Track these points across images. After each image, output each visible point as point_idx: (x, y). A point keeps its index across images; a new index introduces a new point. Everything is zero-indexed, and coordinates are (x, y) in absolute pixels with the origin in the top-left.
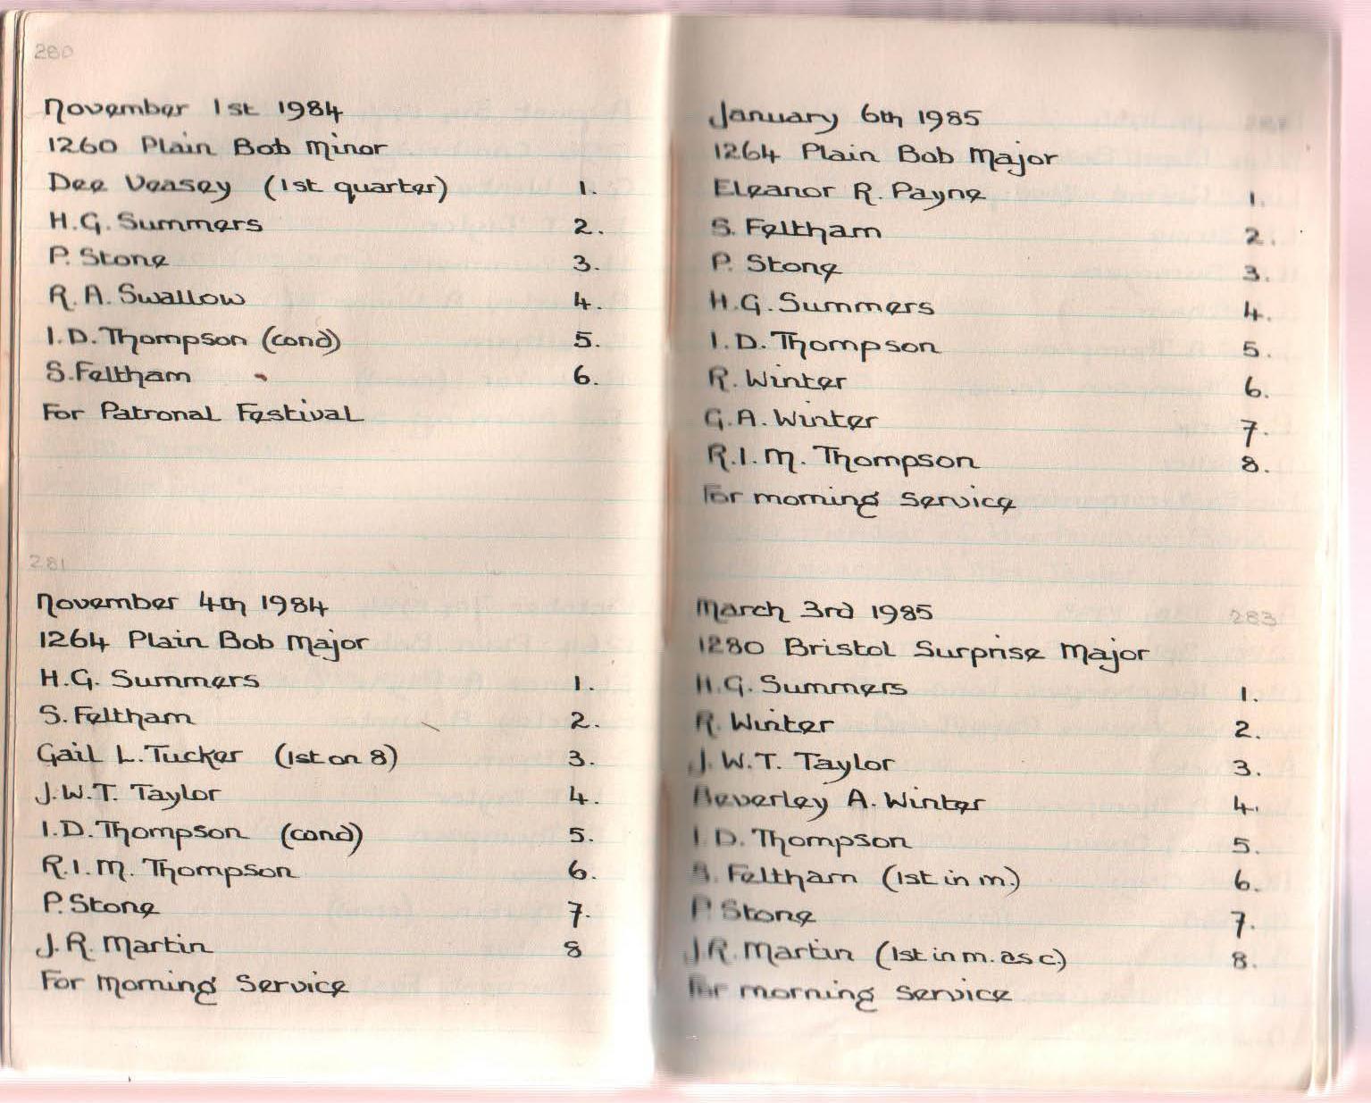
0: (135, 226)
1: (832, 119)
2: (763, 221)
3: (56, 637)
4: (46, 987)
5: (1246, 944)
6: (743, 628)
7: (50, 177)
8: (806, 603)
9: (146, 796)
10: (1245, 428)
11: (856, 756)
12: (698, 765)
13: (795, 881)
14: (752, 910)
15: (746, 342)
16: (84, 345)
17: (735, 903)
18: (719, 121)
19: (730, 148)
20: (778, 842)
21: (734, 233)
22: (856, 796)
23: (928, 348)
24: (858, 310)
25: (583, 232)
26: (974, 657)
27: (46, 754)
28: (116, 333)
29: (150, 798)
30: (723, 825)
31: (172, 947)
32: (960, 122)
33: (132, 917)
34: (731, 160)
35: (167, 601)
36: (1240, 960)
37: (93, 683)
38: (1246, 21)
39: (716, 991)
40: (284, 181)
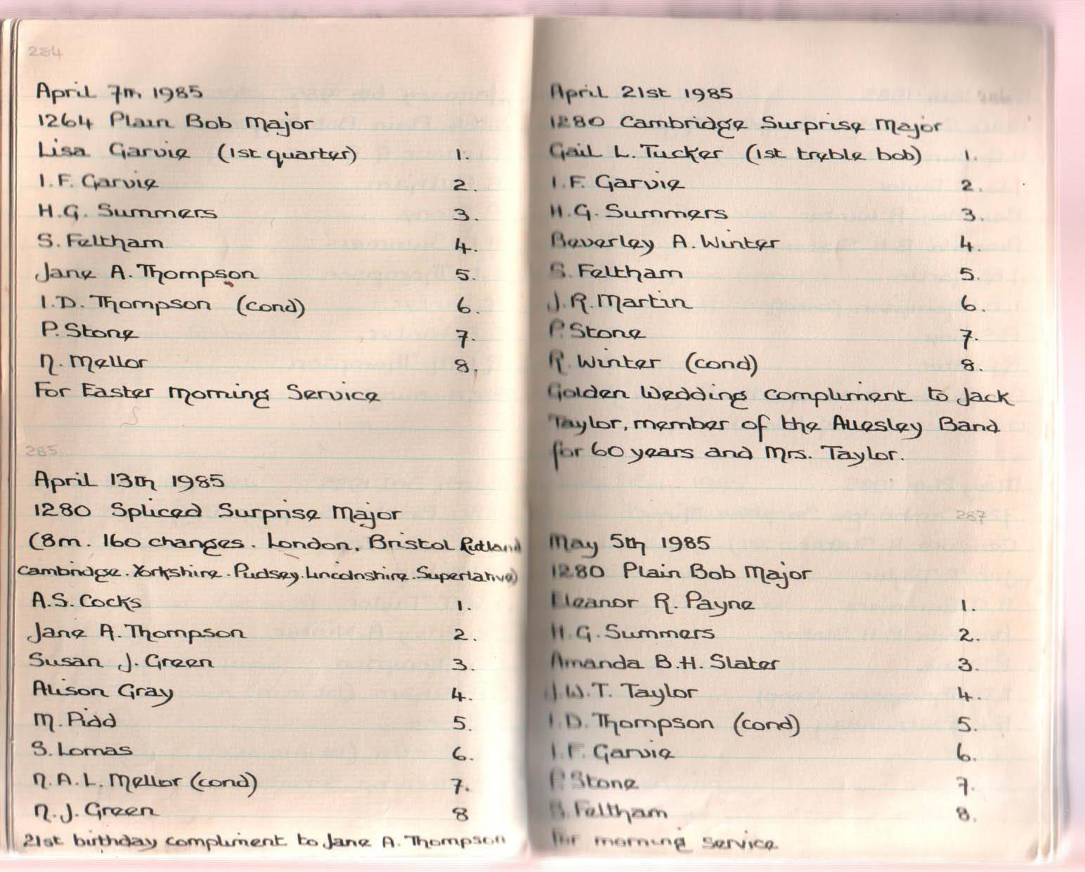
2: (592, 266)
6: (583, 107)
12: (553, 304)
14: (595, 778)
15: (573, 722)
17: (581, 774)
19: (563, 569)
20: (157, 274)
22: (678, 239)
24: (61, 545)
26: (265, 517)
34: (564, 579)
38: (981, 18)
40: (232, 150)
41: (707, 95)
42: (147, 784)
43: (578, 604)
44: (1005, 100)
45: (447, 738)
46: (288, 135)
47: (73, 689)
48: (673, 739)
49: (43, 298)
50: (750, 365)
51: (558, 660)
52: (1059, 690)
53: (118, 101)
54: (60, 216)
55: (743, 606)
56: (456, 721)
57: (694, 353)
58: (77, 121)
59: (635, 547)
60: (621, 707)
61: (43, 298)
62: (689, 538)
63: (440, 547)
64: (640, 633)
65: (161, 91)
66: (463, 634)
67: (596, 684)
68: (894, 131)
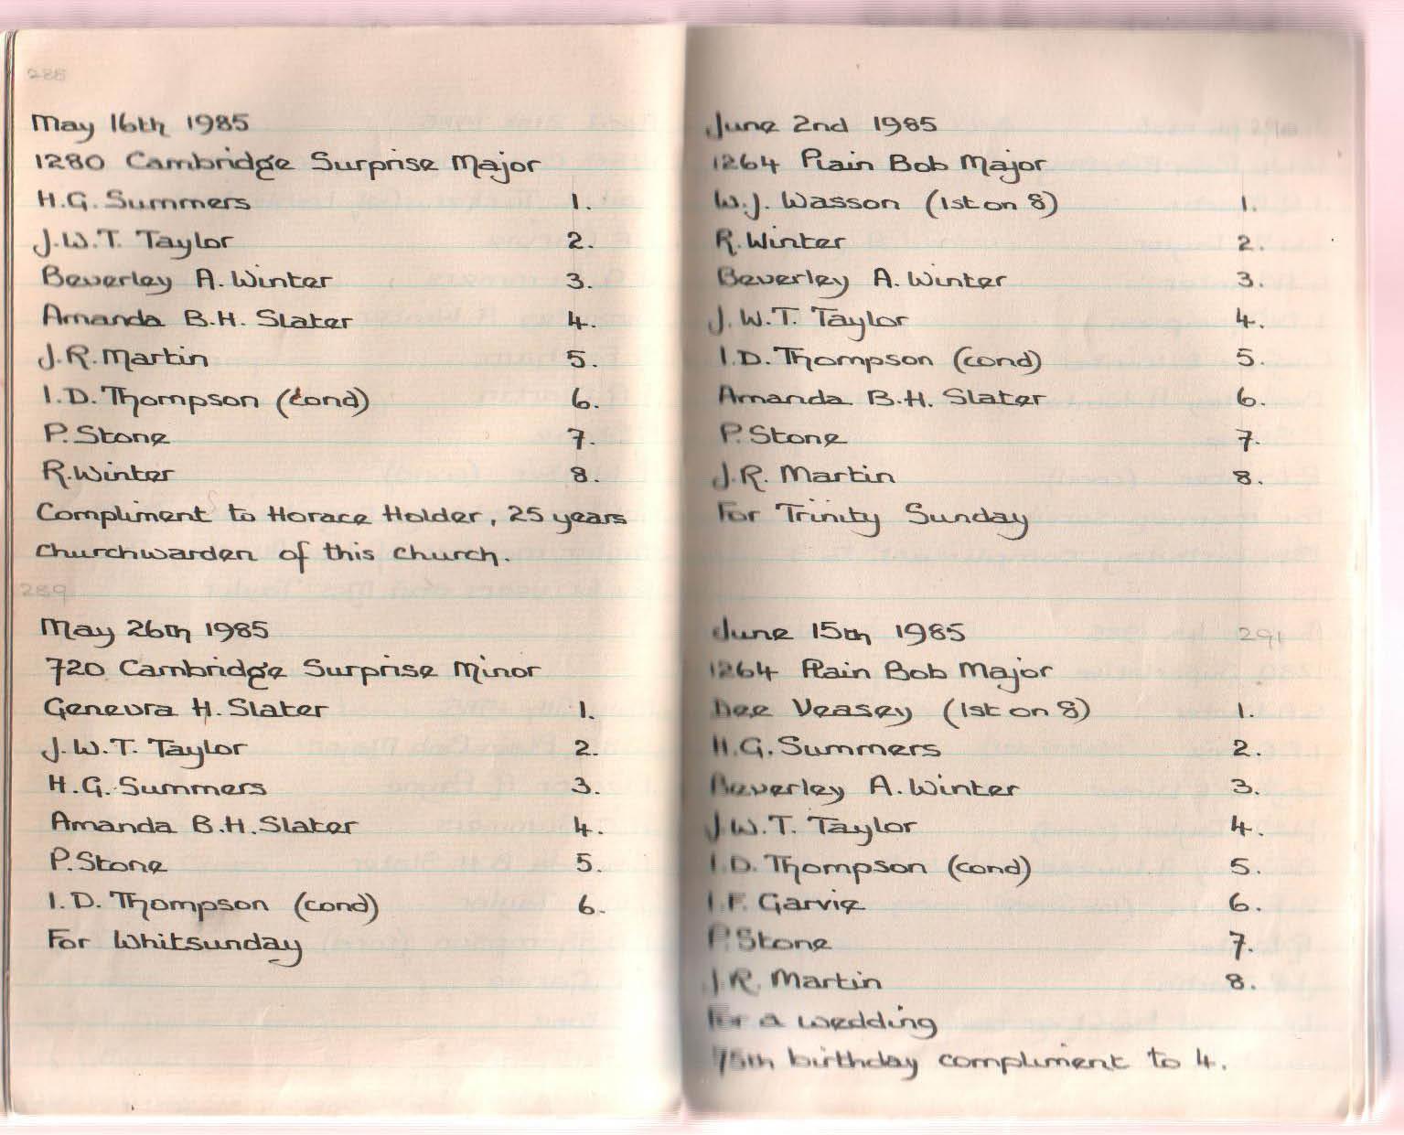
0: (124, 204)
1: (843, 282)
3: (51, 159)
4: (51, 945)
8: (796, 117)
11: (876, 820)
16: (84, 406)
17: (749, 931)
18: (715, 131)
19: (727, 159)
20: (791, 869)
21: (755, 870)
22: (881, 274)
26: (365, 676)
27: (55, 707)
28: (125, 897)
30: (736, 889)
31: (173, 359)
33: (136, 331)
35: (161, 474)
36: (1236, 981)
38: (1269, 24)
39: (737, 1022)
43: (741, 711)
47: (895, 358)
48: (873, 888)
51: (718, 784)
52: (1375, 928)
54: (63, 206)
56: (580, 860)
59: (178, 636)
60: (807, 846)
61: (46, 389)
63: (837, 635)
64: (828, 752)
67: (775, 817)
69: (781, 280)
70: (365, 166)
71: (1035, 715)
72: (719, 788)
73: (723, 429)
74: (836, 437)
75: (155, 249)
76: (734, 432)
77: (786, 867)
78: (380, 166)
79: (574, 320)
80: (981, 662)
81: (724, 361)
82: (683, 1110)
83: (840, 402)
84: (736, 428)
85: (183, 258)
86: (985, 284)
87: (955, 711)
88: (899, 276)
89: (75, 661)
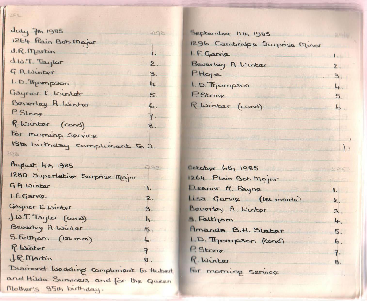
5: (148, 256)
7: (199, 84)
9: (37, 218)
10: (145, 250)
13: (217, 220)
23: (67, 84)
25: (336, 202)
27: (12, 206)
29: (38, 218)
32: (265, 35)
36: (337, 262)
37: (15, 187)
41: (261, 34)
42: (28, 239)
44: (347, 36)
45: (333, 216)
46: (88, 47)
49: (12, 80)
50: (82, 125)
53: (36, 34)
55: (41, 197)
57: (64, 122)
58: (25, 41)
62: (251, 170)
65: (49, 31)
66: (149, 198)
68: (306, 46)
69: (207, 65)
70: (94, 177)
71: (275, 180)
72: (15, 103)
73: (192, 93)
74: (223, 96)
75: (41, 64)
76: (196, 73)
77: (215, 240)
78: (97, 177)
79: (148, 219)
80: (255, 241)
81: (193, 85)
82: (179, 294)
83: (224, 232)
84: (196, 72)
85: (45, 108)
86: (261, 66)
87: (262, 199)
88: (238, 64)
89: (15, 173)
